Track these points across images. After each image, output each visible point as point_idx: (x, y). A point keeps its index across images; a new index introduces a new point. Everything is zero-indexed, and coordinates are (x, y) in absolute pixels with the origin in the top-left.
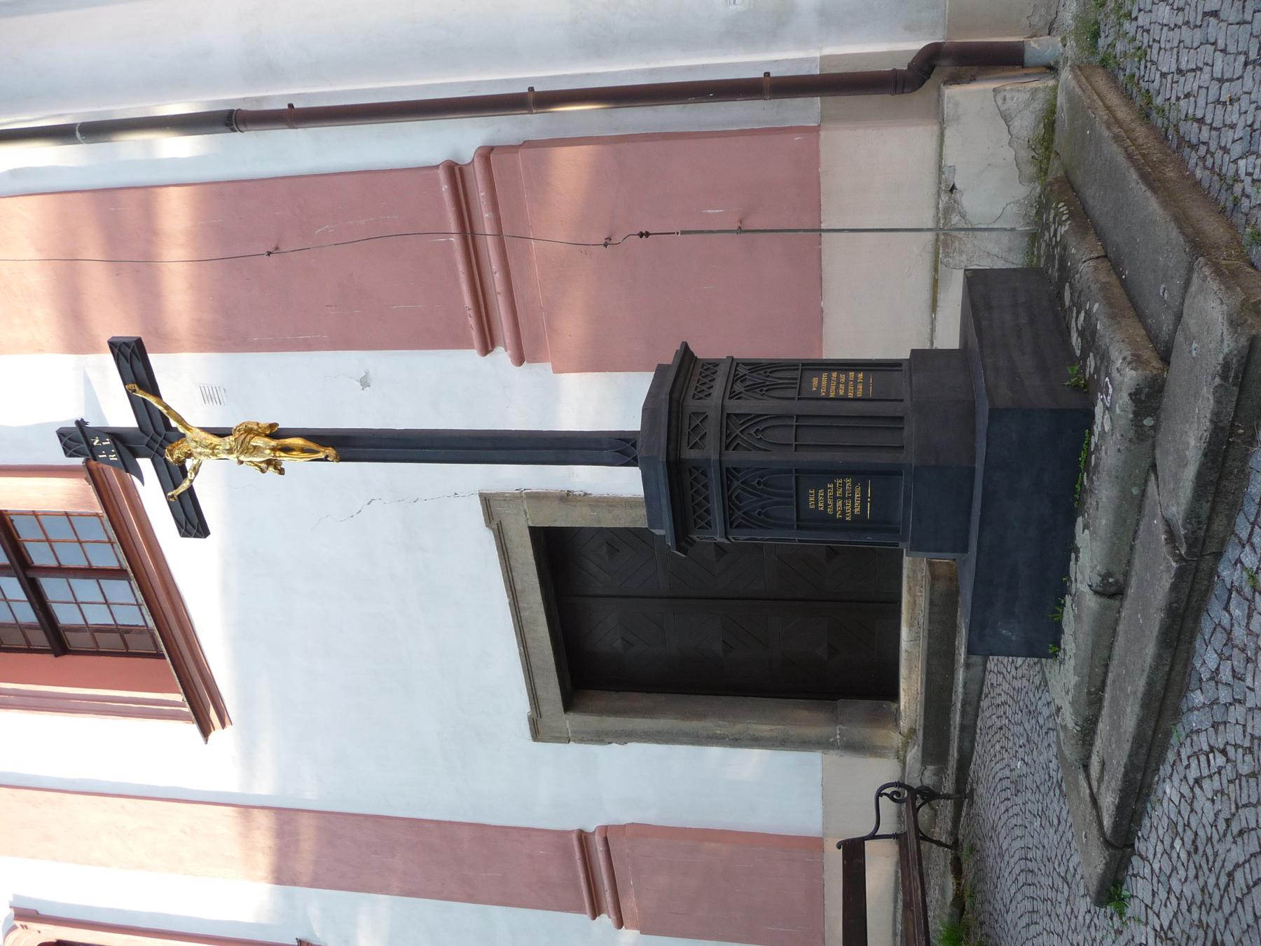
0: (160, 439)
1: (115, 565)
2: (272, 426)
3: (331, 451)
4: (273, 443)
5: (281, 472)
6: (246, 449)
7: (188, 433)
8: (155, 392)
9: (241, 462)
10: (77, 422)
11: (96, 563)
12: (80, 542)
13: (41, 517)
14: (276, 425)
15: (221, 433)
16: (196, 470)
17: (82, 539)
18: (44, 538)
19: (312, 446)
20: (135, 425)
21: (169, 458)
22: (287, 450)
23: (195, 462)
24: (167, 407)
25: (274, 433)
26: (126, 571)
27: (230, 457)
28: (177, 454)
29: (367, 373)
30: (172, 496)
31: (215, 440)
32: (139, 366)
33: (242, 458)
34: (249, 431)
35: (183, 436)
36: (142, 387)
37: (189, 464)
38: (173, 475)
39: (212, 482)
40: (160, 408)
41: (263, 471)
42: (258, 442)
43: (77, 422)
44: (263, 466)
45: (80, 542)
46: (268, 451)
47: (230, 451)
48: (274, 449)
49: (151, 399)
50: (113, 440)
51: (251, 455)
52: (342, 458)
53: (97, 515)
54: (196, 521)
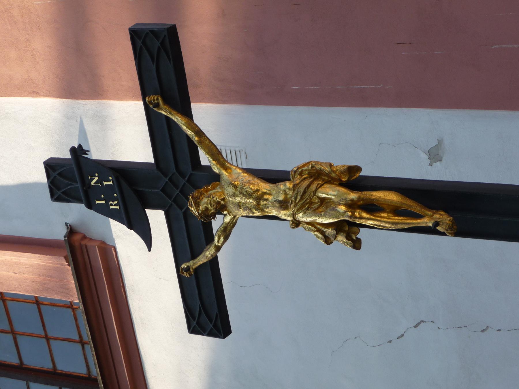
0: (182, 182)
1: (82, 371)
2: (353, 170)
3: (444, 219)
4: (353, 196)
5: (357, 244)
6: (310, 203)
7: (225, 174)
8: (188, 114)
9: (296, 224)
10: (73, 150)
11: (63, 367)
12: (47, 338)
13: (9, 304)
14: (358, 169)
15: (273, 177)
16: (227, 231)
17: (50, 334)
18: (8, 328)
19: (414, 206)
20: (151, 160)
21: (193, 209)
22: (373, 208)
23: (228, 219)
24: (199, 133)
25: (352, 179)
26: (95, 380)
27: (283, 214)
28: (205, 203)
29: (440, 142)
30: (188, 269)
31: (264, 187)
32: (168, 66)
33: (300, 217)
34: (317, 175)
35: (217, 178)
36: (169, 102)
37: (217, 223)
38: (191, 240)
39: (241, 257)
40: (190, 133)
41: (328, 240)
42: (329, 192)
43: (73, 150)
44: (330, 231)
45: (47, 338)
46: (342, 208)
47: (284, 205)
48: (351, 205)
49: (179, 120)
50: (117, 180)
51: (316, 212)
52: (461, 231)
53: (71, 306)
54: (214, 311)
